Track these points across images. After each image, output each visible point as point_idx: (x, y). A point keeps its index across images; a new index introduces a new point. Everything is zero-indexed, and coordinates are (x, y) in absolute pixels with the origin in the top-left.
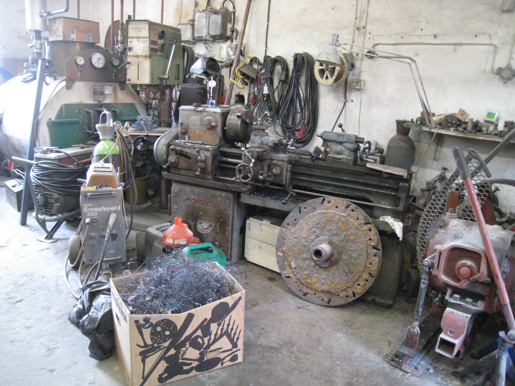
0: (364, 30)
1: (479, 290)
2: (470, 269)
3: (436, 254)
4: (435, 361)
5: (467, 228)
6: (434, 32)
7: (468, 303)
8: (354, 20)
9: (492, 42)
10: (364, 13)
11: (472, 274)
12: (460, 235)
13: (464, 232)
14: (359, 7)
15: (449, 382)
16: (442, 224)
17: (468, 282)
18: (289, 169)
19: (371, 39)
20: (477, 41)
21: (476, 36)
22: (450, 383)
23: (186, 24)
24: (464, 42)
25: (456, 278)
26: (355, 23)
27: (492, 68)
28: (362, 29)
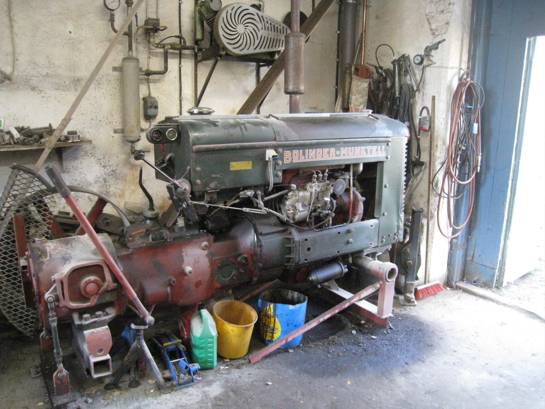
2: (96, 283)
4: (81, 391)
5: (67, 247)
11: (99, 287)
12: (68, 256)
13: (69, 251)
15: (111, 397)
17: (98, 296)
22: (406, 278)
23: (157, 12)
25: (84, 298)
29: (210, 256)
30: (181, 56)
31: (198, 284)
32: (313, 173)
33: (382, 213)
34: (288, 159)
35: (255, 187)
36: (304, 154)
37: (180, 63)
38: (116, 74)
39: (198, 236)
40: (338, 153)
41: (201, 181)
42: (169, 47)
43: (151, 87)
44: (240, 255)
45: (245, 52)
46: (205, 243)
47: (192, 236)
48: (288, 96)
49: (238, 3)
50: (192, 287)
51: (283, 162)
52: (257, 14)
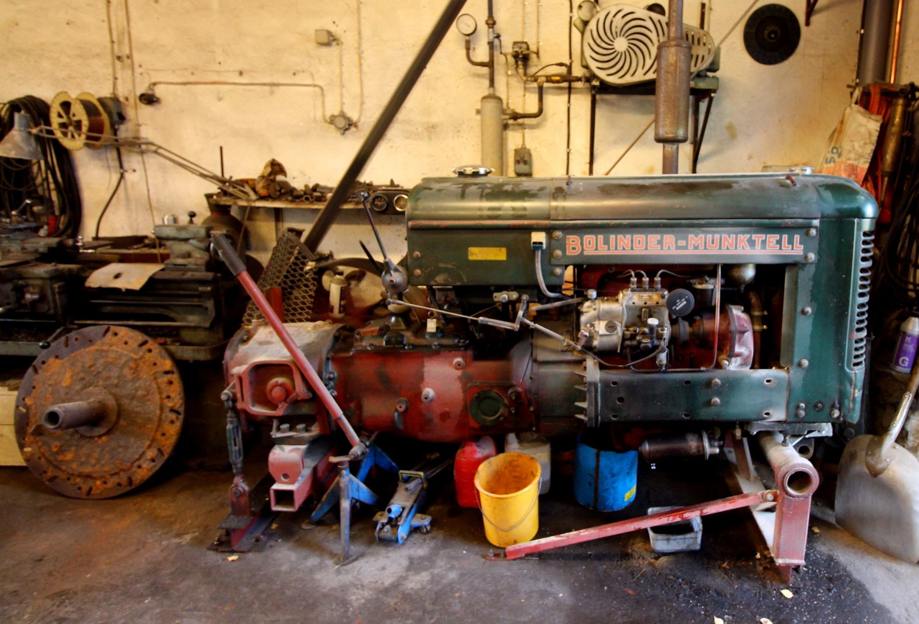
0: (129, 61)
1: (305, 410)
3: (235, 381)
6: (238, 67)
7: (301, 433)
8: (109, 45)
9: (316, 83)
10: (123, 34)
11: (288, 393)
14: (113, 25)
16: (245, 337)
18: (57, 290)
19: (145, 75)
20: (297, 80)
21: (294, 74)
24: (281, 82)
26: (113, 48)
27: (324, 116)
28: (125, 59)
29: (465, 380)
30: (570, 90)
31: (444, 416)
32: (631, 276)
33: (796, 360)
34: (574, 249)
35: (516, 288)
36: (606, 242)
37: (569, 102)
38: (479, 117)
39: (455, 348)
40: (682, 243)
41: (422, 272)
42: (544, 79)
43: (526, 136)
44: (512, 386)
45: (628, 79)
46: (459, 359)
47: (441, 346)
48: (661, 145)
49: (616, 5)
50: (436, 420)
51: (564, 251)
52: (651, 18)
